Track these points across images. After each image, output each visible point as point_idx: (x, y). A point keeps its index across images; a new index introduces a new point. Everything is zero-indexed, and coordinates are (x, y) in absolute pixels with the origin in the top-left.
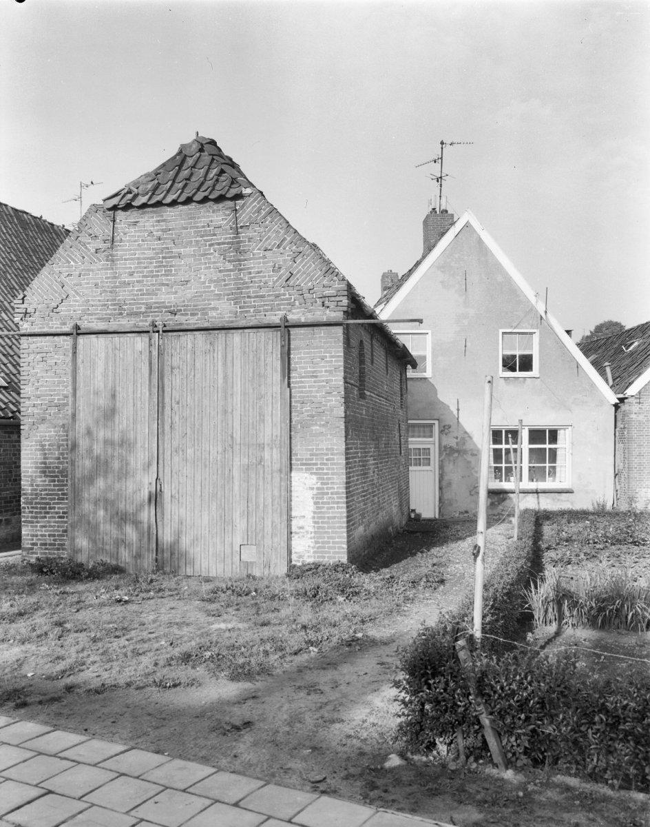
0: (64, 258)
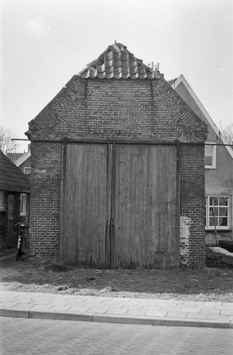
0: (58, 102)
